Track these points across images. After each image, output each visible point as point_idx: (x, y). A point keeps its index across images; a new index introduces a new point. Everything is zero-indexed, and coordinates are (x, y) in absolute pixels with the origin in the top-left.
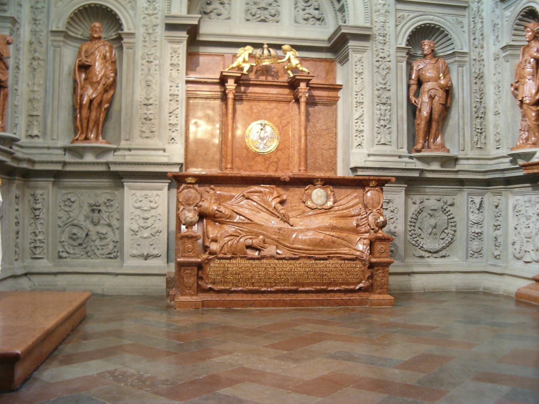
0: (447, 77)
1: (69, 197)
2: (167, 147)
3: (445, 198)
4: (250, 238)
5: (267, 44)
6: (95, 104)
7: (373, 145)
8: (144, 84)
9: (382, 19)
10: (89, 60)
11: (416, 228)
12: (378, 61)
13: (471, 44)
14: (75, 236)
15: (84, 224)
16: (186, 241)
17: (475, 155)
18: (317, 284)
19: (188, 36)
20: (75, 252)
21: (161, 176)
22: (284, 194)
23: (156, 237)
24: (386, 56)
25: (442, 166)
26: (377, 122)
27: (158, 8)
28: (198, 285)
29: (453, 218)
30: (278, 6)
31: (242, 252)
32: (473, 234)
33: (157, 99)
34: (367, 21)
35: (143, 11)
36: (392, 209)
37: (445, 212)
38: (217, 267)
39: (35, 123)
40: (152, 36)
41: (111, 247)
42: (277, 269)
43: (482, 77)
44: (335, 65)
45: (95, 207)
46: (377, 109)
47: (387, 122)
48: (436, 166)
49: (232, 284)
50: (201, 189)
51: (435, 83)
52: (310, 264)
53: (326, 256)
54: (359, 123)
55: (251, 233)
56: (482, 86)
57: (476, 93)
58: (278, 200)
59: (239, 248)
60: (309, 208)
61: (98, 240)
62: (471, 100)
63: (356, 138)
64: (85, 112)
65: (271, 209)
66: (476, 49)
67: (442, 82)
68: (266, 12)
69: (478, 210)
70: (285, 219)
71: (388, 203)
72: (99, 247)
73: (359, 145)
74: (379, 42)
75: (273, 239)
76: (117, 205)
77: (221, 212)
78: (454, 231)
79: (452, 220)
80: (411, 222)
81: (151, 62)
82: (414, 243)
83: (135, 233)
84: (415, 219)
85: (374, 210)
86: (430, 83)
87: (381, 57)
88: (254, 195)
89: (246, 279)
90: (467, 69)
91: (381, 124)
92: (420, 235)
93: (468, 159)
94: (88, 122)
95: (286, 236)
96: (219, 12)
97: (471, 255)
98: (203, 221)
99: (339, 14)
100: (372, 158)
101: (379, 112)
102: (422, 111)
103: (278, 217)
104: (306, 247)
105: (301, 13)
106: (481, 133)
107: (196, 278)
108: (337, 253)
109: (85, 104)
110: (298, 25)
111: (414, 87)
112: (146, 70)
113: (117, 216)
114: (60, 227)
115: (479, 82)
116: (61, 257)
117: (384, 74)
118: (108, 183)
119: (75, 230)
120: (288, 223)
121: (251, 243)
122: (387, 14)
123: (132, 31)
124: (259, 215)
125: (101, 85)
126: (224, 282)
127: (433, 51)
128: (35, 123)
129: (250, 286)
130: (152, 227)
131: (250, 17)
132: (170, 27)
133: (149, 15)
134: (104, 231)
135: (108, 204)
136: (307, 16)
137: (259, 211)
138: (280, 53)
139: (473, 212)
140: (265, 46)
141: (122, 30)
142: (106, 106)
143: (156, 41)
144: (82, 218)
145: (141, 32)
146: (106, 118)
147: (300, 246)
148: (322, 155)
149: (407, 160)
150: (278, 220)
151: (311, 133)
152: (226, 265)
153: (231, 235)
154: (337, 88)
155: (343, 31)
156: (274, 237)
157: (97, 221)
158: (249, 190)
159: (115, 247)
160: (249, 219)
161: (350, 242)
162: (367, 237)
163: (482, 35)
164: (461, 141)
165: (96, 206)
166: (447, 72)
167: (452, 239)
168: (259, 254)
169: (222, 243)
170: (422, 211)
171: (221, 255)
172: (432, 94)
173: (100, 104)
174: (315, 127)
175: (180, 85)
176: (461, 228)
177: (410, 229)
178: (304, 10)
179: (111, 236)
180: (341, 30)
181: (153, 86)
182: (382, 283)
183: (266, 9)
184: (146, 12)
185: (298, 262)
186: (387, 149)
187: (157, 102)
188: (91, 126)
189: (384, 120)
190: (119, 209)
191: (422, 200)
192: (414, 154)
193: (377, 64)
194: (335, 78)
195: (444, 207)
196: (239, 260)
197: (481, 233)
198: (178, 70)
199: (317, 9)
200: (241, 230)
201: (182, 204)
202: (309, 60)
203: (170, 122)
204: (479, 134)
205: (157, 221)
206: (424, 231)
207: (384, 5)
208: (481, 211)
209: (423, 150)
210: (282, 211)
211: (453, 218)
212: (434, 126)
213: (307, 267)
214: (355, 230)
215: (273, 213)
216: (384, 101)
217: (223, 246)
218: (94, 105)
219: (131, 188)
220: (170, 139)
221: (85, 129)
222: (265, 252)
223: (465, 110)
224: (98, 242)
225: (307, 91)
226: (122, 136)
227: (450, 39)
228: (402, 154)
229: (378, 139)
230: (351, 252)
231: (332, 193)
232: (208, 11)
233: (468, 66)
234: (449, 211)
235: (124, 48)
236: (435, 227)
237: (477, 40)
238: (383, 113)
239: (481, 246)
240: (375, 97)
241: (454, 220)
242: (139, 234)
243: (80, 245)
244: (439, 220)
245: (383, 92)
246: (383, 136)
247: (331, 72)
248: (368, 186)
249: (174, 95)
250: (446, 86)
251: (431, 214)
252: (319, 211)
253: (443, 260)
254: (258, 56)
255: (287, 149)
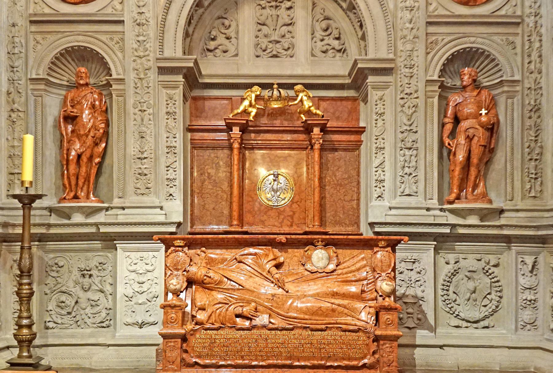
0: (493, 111)
1: (56, 261)
2: (165, 204)
3: (487, 257)
4: (241, 306)
5: (278, 84)
6: (84, 159)
7: (395, 197)
8: (137, 136)
9: (409, 47)
10: (75, 111)
11: (451, 292)
12: (402, 98)
13: (525, 70)
14: (63, 304)
15: (73, 290)
16: (169, 311)
17: (527, 205)
18: (314, 358)
19: (184, 80)
20: (63, 321)
21: (148, 237)
22: (282, 256)
23: (153, 303)
24: (413, 92)
25: (481, 220)
26: (400, 170)
27: (149, 49)
28: (183, 360)
29: (498, 281)
30: (293, 37)
31: (231, 322)
32: (525, 302)
33: (152, 152)
34: (390, 51)
35: (133, 53)
36: (418, 270)
37: (487, 274)
38: (203, 339)
39: (16, 181)
40: (144, 81)
41: (103, 314)
42: (269, 341)
43: (539, 109)
44: (359, 104)
45: (86, 272)
46: (400, 155)
47: (413, 169)
48: (473, 220)
49: (220, 357)
50: (192, 252)
51: (474, 120)
52: (305, 335)
53: (323, 327)
54: (380, 171)
55: (242, 300)
56: (539, 120)
57: (530, 129)
58: (274, 263)
59: (227, 317)
60: (308, 271)
61: (89, 308)
62: (522, 139)
63: (376, 188)
64: (73, 168)
65: (264, 274)
66: (532, 75)
67: (484, 119)
68: (278, 45)
69: (531, 272)
70: (279, 284)
71: (414, 262)
72: (90, 315)
73: (379, 196)
74: (405, 76)
75: (266, 307)
76: (110, 268)
77: (210, 277)
78: (499, 297)
79: (497, 284)
80: (443, 285)
81: (145, 111)
82: (448, 309)
83: (130, 299)
84: (448, 282)
85: (383, 274)
86: (469, 121)
87: (406, 94)
88: (247, 258)
89: (234, 351)
90: (518, 100)
91: (405, 172)
92: (455, 300)
93: (517, 211)
94: (77, 178)
95: (280, 303)
96: (225, 48)
97: (522, 327)
98: (191, 287)
99: (362, 43)
100: (393, 212)
101: (402, 159)
102: (457, 155)
103: (273, 282)
104: (302, 316)
105: (319, 44)
106: (536, 179)
107: (179, 351)
108: (337, 324)
109: (73, 160)
110: (316, 58)
111: (449, 127)
112: (139, 119)
113: (110, 280)
114: (46, 294)
115: (535, 116)
116: (47, 328)
117: (410, 114)
118: (100, 245)
119: (63, 298)
120: (283, 289)
121: (241, 312)
122: (417, 40)
123: (121, 77)
124: (251, 280)
125: (90, 137)
126: (211, 356)
127: (475, 81)
128: (16, 181)
129: (239, 360)
130: (148, 291)
131: (260, 52)
132: (162, 71)
133: (140, 57)
134: (96, 298)
135: (100, 268)
136: (324, 49)
137: (253, 275)
138: (291, 93)
139: (523, 275)
140: (275, 86)
141: (111, 75)
142: (97, 160)
143: (148, 88)
144: (71, 284)
145: (131, 77)
146: (99, 174)
147: (295, 315)
148: (343, 207)
149: (438, 212)
150: (272, 285)
151: (330, 183)
152: (213, 336)
153: (220, 303)
154: (360, 131)
155: (360, 66)
156: (267, 304)
157: (87, 287)
158: (242, 253)
159: (108, 314)
160: (240, 285)
161: (354, 310)
162: (373, 305)
163: (540, 56)
164: (509, 189)
165: (87, 271)
166: (492, 105)
167: (497, 307)
168: (250, 324)
169: (210, 311)
170: (458, 273)
171: (208, 326)
172: (470, 134)
173: (91, 159)
174: (335, 176)
175: (177, 136)
176: (508, 293)
177: (442, 294)
178: (322, 40)
179: (104, 302)
180: (357, 64)
181: (148, 138)
182: (389, 360)
183: (278, 42)
184: (136, 54)
185: (293, 332)
186: (412, 201)
187: (152, 156)
188: (80, 183)
189: (409, 167)
190: (112, 273)
191: (456, 260)
192: (445, 207)
193: (402, 102)
194: (358, 120)
195: (486, 269)
196: (227, 331)
197: (534, 301)
198: (175, 119)
199: (338, 39)
200: (231, 297)
201: (169, 269)
202: (328, 100)
203: (168, 177)
204: (533, 181)
205: (154, 285)
206: (461, 296)
207: (412, 29)
208: (534, 273)
209: (456, 201)
210: (277, 276)
211: (498, 281)
212: (473, 172)
213: (303, 339)
214: (360, 297)
215: (267, 278)
216: (409, 145)
217: (211, 315)
218: (82, 161)
219: (125, 250)
220: (168, 195)
221: (73, 187)
222: (258, 321)
223: (515, 152)
224: (89, 310)
225: (321, 137)
226: (115, 194)
227: (497, 65)
228: (430, 206)
229: (401, 190)
230: (353, 323)
231: (335, 255)
232: (212, 48)
233: (520, 97)
234: (493, 273)
235: (114, 96)
236: (474, 292)
237: (533, 63)
238: (407, 158)
239: (534, 316)
240: (398, 140)
241: (500, 284)
242: (134, 300)
243: (69, 313)
244: (480, 283)
245: (408, 135)
246: (407, 185)
247: (354, 113)
248: (377, 246)
249: (171, 147)
250: (488, 123)
251: (468, 275)
252: (319, 275)
253: (486, 331)
254: (266, 97)
255: (303, 202)
